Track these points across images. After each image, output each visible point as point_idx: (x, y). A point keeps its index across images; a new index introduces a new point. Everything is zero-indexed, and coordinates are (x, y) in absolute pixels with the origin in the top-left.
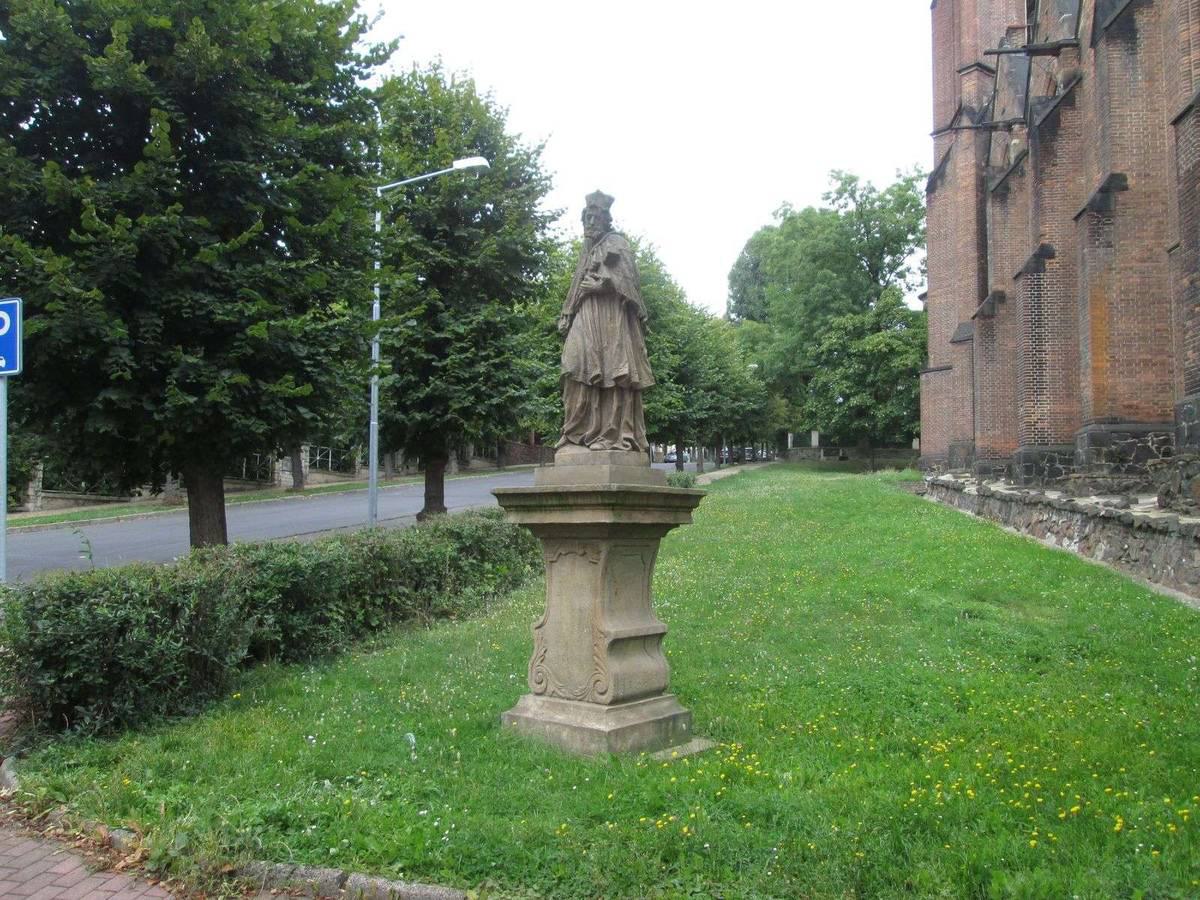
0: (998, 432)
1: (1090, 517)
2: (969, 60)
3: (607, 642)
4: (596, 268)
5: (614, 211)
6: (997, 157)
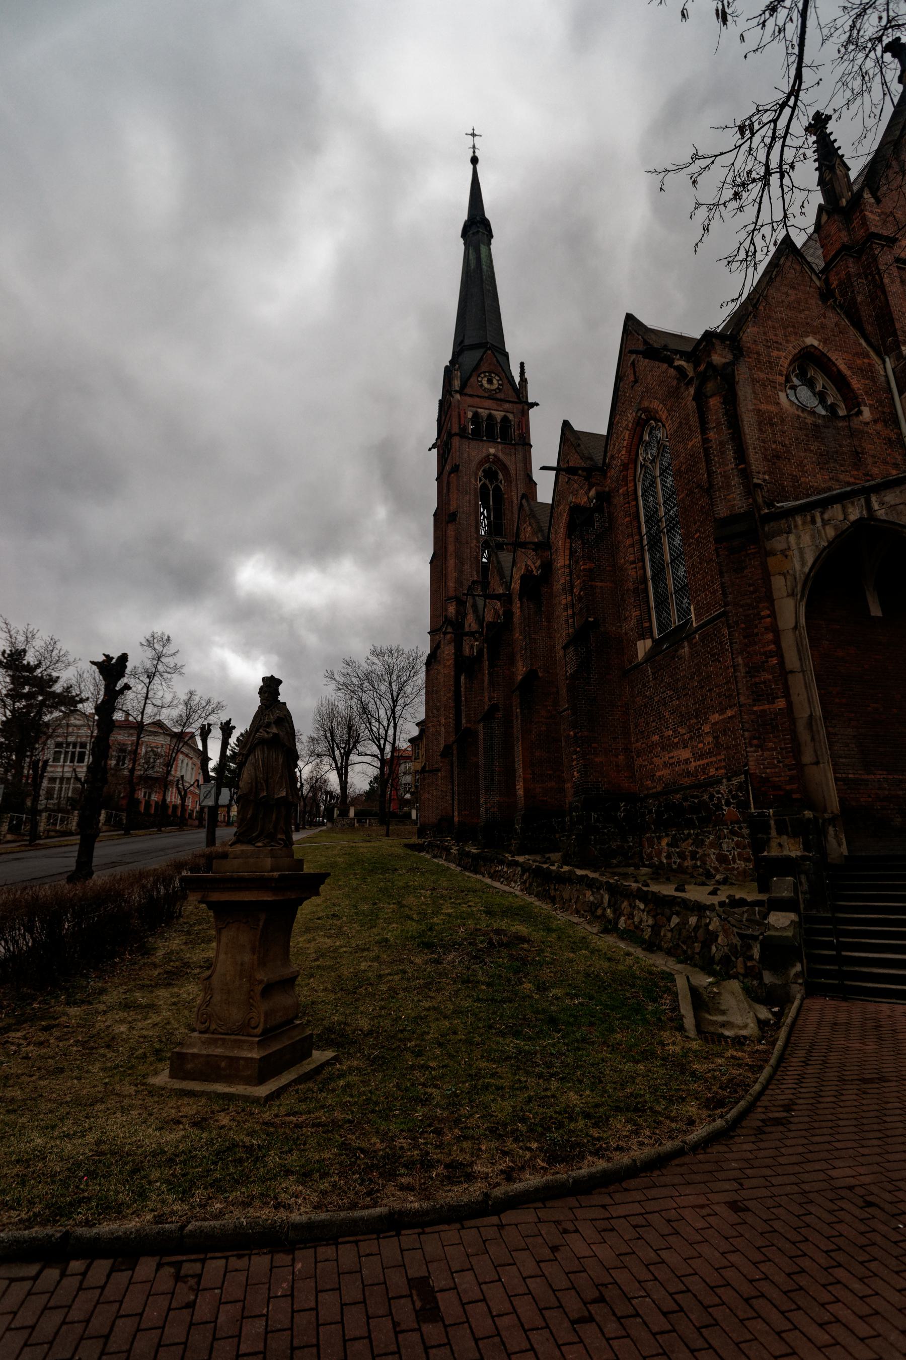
0: (467, 813)
1: (525, 868)
2: (451, 593)
3: (261, 987)
4: (268, 725)
5: (281, 688)
6: (467, 651)
